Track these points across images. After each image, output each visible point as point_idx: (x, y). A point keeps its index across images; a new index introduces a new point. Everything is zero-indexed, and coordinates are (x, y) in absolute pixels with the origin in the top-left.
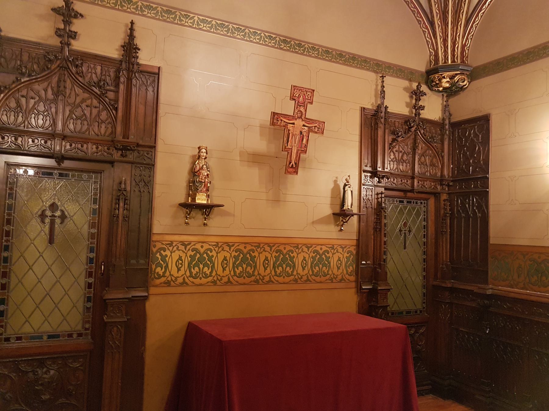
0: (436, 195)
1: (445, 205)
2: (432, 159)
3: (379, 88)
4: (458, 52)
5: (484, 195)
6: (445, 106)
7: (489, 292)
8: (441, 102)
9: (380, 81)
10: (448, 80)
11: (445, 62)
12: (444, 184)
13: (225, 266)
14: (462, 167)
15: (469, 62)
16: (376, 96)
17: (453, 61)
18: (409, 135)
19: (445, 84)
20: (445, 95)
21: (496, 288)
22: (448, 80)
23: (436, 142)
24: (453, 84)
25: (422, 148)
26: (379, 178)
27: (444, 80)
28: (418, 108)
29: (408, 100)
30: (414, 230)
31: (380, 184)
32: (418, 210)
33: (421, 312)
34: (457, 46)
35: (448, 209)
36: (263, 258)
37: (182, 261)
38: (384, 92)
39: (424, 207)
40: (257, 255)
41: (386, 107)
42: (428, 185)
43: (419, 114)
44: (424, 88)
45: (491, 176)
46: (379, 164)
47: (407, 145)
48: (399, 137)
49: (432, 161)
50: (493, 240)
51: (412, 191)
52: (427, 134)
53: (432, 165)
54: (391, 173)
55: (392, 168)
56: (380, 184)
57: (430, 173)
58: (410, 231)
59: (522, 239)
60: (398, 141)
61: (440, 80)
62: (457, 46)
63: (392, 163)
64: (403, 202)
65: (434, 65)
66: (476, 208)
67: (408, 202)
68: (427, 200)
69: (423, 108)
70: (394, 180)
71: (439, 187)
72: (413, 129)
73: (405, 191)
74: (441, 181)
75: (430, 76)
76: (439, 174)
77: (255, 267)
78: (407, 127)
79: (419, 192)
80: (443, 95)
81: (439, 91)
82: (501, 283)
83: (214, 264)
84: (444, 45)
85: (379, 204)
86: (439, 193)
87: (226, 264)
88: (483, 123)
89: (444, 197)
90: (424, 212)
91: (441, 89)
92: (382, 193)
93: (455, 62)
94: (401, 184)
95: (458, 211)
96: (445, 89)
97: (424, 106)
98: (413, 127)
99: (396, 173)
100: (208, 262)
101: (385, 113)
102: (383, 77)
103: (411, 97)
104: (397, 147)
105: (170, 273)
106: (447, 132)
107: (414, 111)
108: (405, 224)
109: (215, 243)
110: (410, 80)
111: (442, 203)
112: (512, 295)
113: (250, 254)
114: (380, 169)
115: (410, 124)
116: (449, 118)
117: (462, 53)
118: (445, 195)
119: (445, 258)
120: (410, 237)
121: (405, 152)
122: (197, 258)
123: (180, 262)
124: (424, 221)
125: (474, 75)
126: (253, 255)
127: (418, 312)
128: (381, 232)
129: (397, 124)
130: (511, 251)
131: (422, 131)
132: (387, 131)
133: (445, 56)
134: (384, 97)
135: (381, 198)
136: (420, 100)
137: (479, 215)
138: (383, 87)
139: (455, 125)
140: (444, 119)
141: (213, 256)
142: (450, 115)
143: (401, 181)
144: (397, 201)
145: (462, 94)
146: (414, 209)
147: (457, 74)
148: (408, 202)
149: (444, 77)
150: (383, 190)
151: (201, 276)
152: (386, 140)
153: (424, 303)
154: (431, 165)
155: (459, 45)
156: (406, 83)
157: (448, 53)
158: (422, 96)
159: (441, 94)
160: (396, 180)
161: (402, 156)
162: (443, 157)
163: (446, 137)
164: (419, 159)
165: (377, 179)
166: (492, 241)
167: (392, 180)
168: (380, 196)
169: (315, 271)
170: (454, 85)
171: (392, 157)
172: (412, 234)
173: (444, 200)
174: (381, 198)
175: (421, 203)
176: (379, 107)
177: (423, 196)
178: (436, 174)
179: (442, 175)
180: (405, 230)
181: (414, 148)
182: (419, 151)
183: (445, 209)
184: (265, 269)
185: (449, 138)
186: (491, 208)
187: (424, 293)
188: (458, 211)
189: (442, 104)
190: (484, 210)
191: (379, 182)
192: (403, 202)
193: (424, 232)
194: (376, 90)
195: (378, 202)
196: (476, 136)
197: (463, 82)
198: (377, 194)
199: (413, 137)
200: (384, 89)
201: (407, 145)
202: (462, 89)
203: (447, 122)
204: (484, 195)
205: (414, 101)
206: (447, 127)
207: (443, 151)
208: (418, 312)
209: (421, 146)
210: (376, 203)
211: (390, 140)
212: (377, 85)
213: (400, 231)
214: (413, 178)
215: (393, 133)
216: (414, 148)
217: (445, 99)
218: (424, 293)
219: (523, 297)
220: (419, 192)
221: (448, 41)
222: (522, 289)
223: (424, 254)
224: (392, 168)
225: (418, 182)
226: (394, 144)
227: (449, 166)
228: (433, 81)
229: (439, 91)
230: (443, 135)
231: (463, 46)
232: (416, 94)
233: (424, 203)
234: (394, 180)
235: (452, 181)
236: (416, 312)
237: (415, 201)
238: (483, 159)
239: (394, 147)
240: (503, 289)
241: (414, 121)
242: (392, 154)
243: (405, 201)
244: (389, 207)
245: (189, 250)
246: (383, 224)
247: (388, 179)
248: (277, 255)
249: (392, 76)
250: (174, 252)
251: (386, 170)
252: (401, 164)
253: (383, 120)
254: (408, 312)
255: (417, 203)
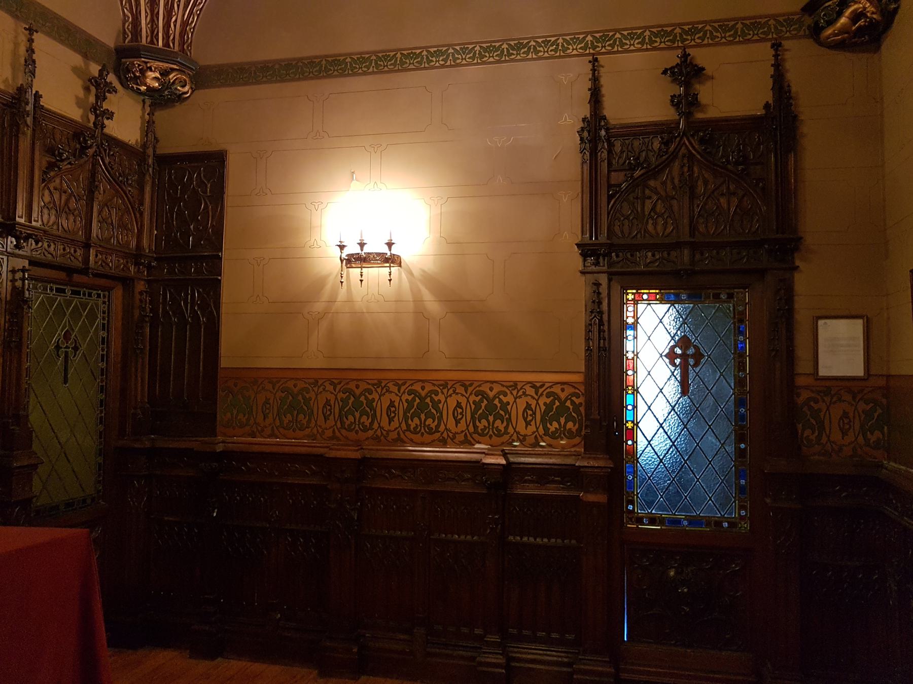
0: (127, 282)
1: (141, 301)
2: (122, 216)
3: (22, 50)
4: (175, 30)
5: (213, 286)
6: (148, 122)
7: (220, 448)
8: (140, 113)
9: (23, 38)
10: (157, 75)
11: (152, 42)
12: (142, 264)
13: (460, 417)
14: (176, 236)
15: (194, 53)
16: (14, 67)
17: (166, 44)
18: (82, 161)
19: (152, 79)
20: (148, 102)
21: (230, 440)
22: (157, 75)
23: (130, 185)
24: (166, 85)
25: (104, 192)
26: (18, 239)
27: (151, 75)
28: (102, 115)
29: (81, 94)
30: (84, 347)
31: (21, 252)
32: (92, 309)
33: (93, 500)
34: (174, 19)
35: (148, 310)
36: (386, 404)
37: (462, 408)
38: (34, 61)
39: (104, 303)
40: (376, 397)
41: (37, 96)
42: (114, 262)
43: (103, 126)
44: (111, 78)
45: (225, 254)
46: (20, 209)
47: (77, 181)
48: (62, 161)
49: (121, 219)
50: (225, 361)
51: (85, 271)
52: (115, 167)
53: (123, 226)
54: (45, 231)
55: (45, 221)
56: (21, 252)
57: (118, 241)
58: (76, 349)
59: (272, 357)
60: (60, 169)
61: (143, 72)
62: (174, 19)
63: (46, 211)
64: (63, 291)
65: (131, 41)
66: (199, 308)
67: (74, 292)
68: (109, 289)
69: (110, 116)
70: (49, 246)
71: (132, 268)
72: (90, 152)
73: (70, 271)
74: (136, 257)
75: (124, 60)
76: (133, 244)
77: (440, 418)
78: (78, 146)
79: (96, 275)
80: (144, 101)
81: (138, 92)
82: (241, 431)
83: (441, 414)
84: (152, 11)
85: (18, 293)
86: (132, 280)
87: (461, 413)
88: (214, 163)
89: (140, 286)
90: (104, 313)
91: (143, 88)
92: (23, 270)
93: (169, 46)
94: (63, 255)
95: (165, 313)
96: (150, 90)
97: (113, 113)
98: (91, 147)
99: (55, 232)
100: (433, 411)
101: (35, 107)
102: (31, 31)
103: (87, 89)
104: (58, 181)
105: (515, 429)
106: (151, 170)
107: (92, 118)
108: (67, 336)
109: (312, 381)
110: (85, 56)
111: (138, 297)
112: (256, 449)
113: (303, 395)
114: (22, 221)
115: (85, 141)
116: (154, 147)
117: (183, 32)
118: (143, 283)
119: (139, 397)
120: (76, 360)
121: (72, 194)
122: (415, 404)
123: (460, 410)
124: (103, 329)
125: (203, 78)
126: (370, 397)
127: (89, 501)
128: (20, 351)
129: (58, 137)
130: (253, 378)
131: (107, 160)
132: (38, 144)
133: (152, 32)
134: (33, 73)
135: (23, 279)
136: (105, 98)
137: (203, 320)
138: (31, 51)
139: (164, 161)
140: (144, 146)
141: (440, 401)
142: (157, 140)
143: (64, 249)
144: (51, 290)
145: (179, 108)
146: (84, 306)
147: (173, 70)
148: (74, 292)
149: (150, 69)
150: (26, 263)
151: (491, 432)
152: (37, 163)
153: (99, 482)
154: (119, 226)
155: (177, 17)
156: (77, 59)
157: (157, 26)
158: (109, 92)
159: (142, 98)
160: (53, 246)
161: (67, 201)
162: (141, 214)
163: (147, 178)
164: (100, 213)
165: (13, 240)
166: (224, 363)
167: (46, 245)
168: (19, 275)
169: (347, 423)
170: (167, 88)
171: (47, 198)
172: (80, 354)
173: (141, 293)
174: (23, 279)
175: (99, 296)
176: (21, 90)
177: (102, 282)
178: (128, 243)
179: (139, 246)
180: (67, 347)
181: (91, 190)
182: (100, 197)
183: (144, 309)
184: (391, 420)
185: (153, 182)
186: (224, 309)
187: (100, 464)
188: (165, 313)
189: (142, 117)
190: (212, 312)
191: (17, 246)
192: (63, 291)
193: (103, 350)
194: (15, 53)
195: (14, 288)
196: (201, 184)
197: (183, 86)
198: (14, 271)
199: (89, 166)
200: (34, 56)
201: (77, 181)
202: (180, 98)
203: (150, 151)
204: (212, 286)
205: (92, 99)
206: (150, 161)
207: (141, 203)
208: (89, 501)
209: (103, 186)
210: (9, 289)
211: (45, 164)
212: (16, 45)
213: (58, 347)
214: (87, 246)
215: (50, 150)
216: (91, 190)
217: (148, 110)
218: (100, 464)
219: (275, 449)
220: (96, 275)
221: (158, 5)
222: (270, 436)
223: (102, 392)
224: (45, 221)
225: (97, 256)
226: (52, 174)
227: (151, 231)
228: (129, 71)
229: (138, 92)
230: (142, 175)
231: (185, 24)
232: (97, 86)
233: (104, 296)
234: (49, 246)
235: (156, 259)
236: (84, 501)
237: (87, 291)
238: (212, 226)
239: (51, 180)
240: (239, 440)
241: (93, 137)
242: (47, 192)
243: (68, 290)
244: (36, 297)
245: (404, 392)
246: (25, 335)
247: (37, 243)
248: (283, 395)
249: (48, 34)
250: (451, 396)
251: (34, 224)
252: (64, 215)
253: (29, 120)
254: (68, 505)
255: (90, 295)
